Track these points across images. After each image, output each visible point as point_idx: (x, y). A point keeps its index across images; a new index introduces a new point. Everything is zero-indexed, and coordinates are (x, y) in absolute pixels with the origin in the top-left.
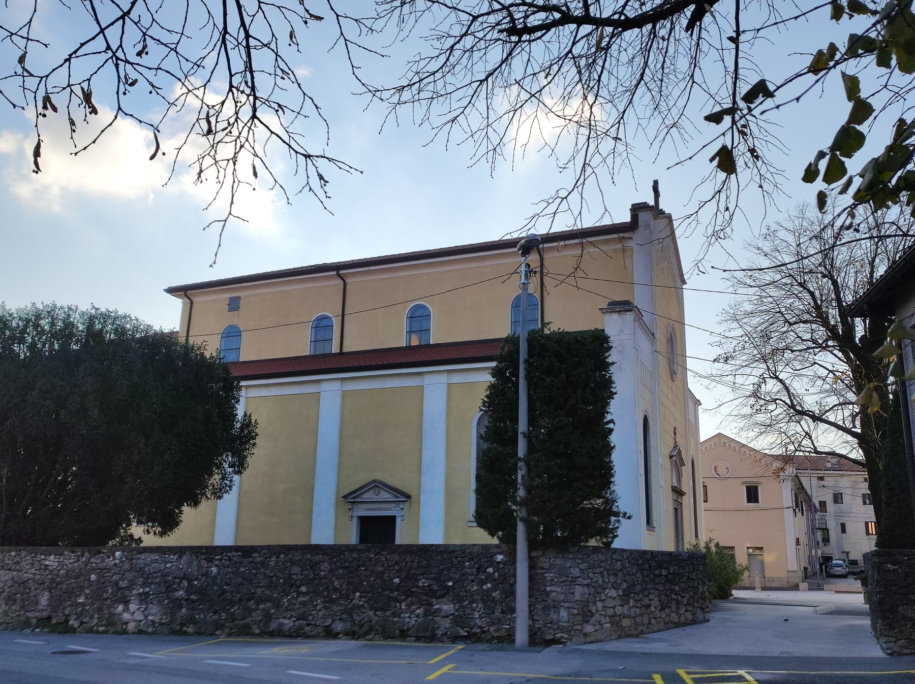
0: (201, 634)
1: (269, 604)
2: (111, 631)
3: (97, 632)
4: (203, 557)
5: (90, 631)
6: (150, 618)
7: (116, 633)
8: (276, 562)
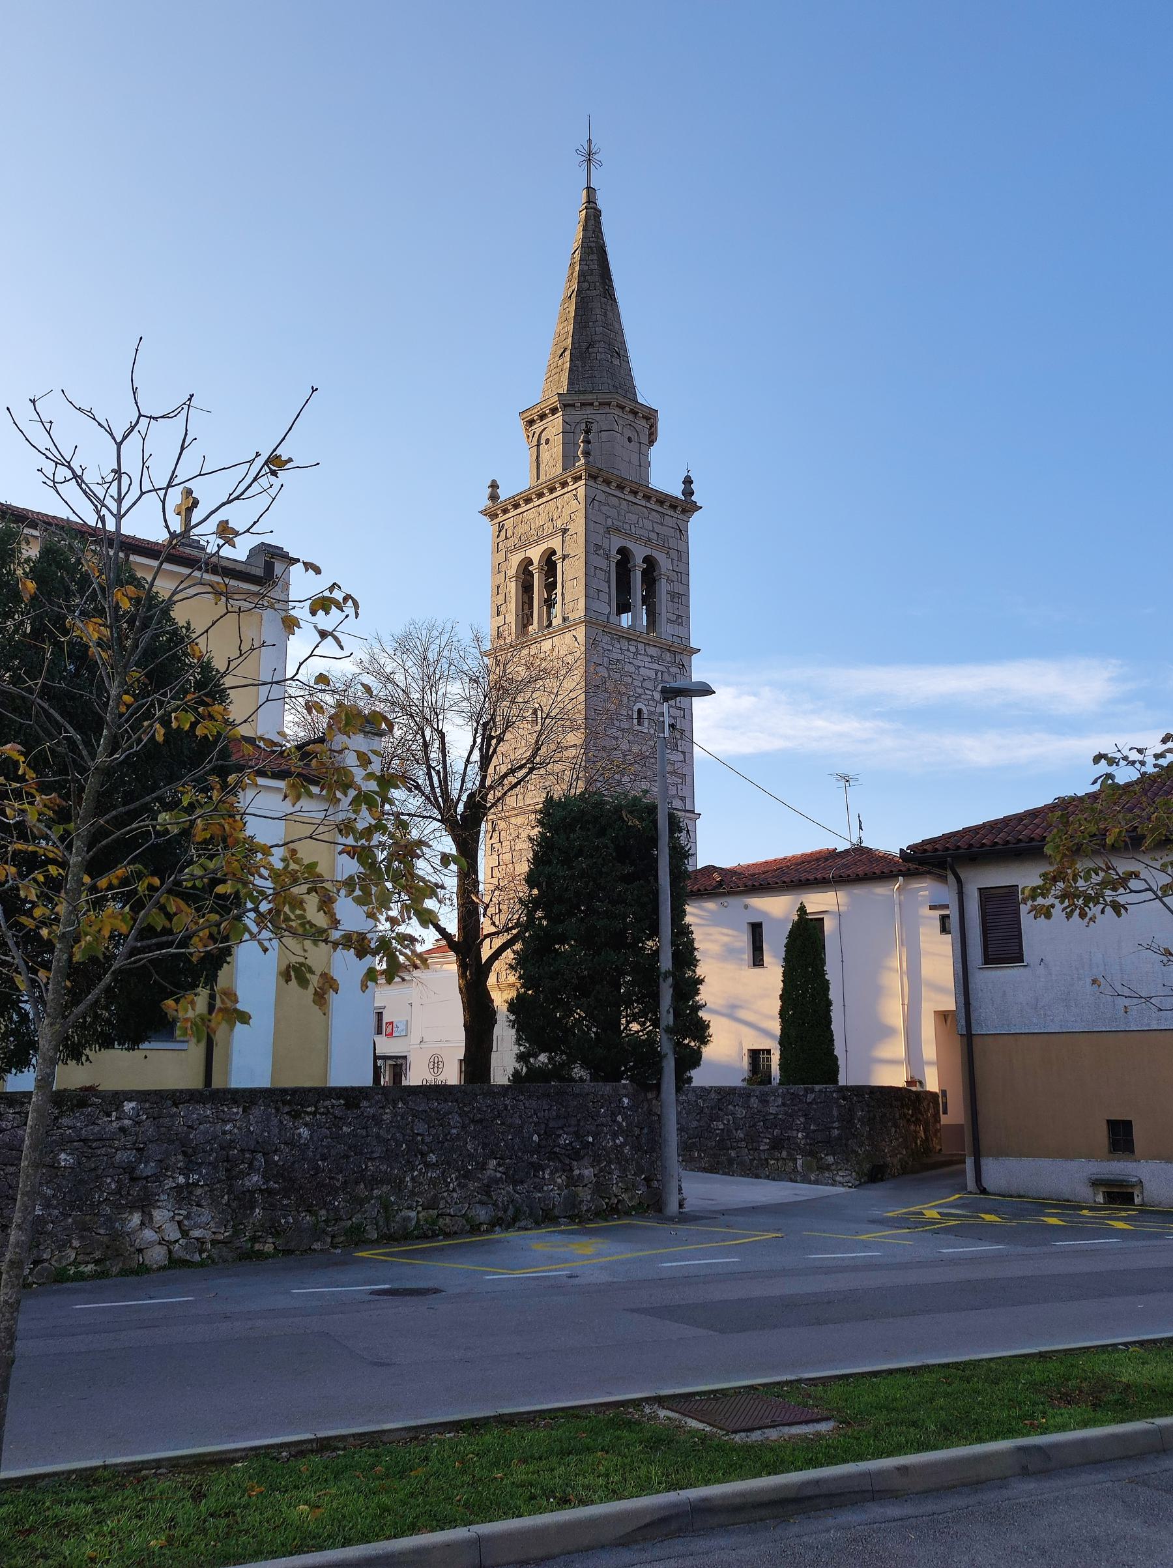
0: (288, 1252)
1: (386, 1188)
2: (115, 1270)
3: (80, 1277)
4: (287, 1109)
5: (60, 1277)
6: (196, 1233)
7: (124, 1273)
8: (395, 1115)
